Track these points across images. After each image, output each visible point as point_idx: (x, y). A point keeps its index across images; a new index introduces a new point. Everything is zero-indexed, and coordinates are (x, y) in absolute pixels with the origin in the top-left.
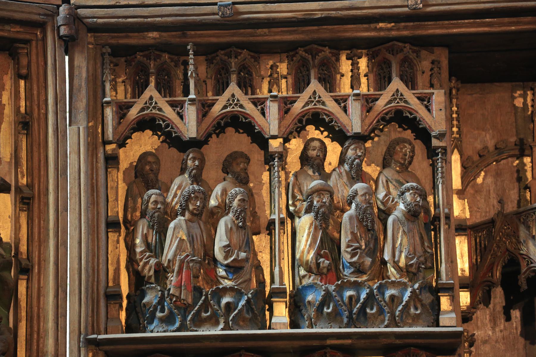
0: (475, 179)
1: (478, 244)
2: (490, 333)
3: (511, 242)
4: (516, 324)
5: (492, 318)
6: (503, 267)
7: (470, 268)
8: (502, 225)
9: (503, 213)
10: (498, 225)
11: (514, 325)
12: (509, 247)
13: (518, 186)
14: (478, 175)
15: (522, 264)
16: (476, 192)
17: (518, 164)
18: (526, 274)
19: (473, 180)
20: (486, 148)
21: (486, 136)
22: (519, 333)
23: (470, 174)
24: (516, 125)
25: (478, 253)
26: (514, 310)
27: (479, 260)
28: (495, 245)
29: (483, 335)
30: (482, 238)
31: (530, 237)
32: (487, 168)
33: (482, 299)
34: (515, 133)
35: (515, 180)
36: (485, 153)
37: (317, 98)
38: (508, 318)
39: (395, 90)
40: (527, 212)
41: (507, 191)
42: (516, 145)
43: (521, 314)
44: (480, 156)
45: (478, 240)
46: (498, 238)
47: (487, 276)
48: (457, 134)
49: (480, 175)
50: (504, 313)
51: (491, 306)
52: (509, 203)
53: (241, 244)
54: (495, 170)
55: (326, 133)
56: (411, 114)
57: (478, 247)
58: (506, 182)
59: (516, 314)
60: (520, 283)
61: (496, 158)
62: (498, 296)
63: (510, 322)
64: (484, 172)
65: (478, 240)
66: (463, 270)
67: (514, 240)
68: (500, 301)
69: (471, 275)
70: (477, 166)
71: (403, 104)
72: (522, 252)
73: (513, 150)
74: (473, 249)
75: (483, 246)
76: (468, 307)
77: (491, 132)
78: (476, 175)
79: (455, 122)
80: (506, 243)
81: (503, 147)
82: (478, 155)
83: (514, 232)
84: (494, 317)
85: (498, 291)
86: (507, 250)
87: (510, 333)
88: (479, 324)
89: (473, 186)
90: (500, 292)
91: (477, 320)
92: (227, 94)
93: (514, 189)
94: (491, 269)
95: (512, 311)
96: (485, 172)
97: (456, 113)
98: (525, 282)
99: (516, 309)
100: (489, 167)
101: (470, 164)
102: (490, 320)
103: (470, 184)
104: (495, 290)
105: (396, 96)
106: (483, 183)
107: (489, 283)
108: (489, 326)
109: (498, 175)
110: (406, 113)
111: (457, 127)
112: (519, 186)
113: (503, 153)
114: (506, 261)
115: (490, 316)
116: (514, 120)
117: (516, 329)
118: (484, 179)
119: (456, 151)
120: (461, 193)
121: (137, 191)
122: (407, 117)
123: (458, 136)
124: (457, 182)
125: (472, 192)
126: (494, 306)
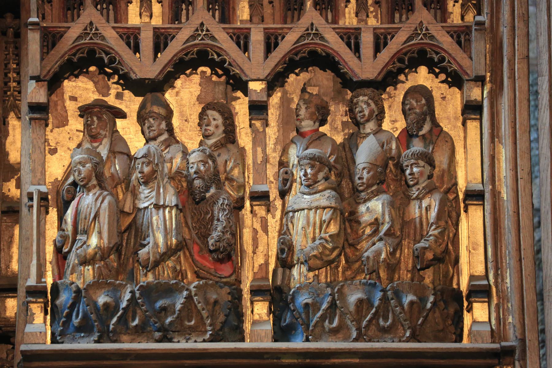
37: (93, 30)
39: (89, 22)
53: (93, 224)
55: (443, 77)
56: (219, 55)
71: (210, 42)
92: (195, 22)
105: (310, 31)
110: (100, 53)
122: (213, 59)
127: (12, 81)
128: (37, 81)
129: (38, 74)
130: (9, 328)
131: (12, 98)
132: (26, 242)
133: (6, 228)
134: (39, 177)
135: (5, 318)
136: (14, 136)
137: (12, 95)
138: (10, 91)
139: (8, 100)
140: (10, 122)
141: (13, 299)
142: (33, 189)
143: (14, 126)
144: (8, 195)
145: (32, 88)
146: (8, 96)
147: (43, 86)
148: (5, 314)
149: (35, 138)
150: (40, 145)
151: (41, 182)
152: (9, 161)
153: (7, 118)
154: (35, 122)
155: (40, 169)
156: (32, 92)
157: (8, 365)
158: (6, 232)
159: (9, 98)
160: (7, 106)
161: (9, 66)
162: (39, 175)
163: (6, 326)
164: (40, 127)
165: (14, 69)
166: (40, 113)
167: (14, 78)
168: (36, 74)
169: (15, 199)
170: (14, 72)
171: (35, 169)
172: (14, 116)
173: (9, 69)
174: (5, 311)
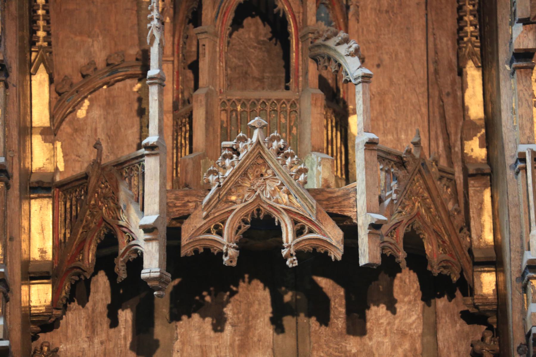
0: (74, 110)
1: (68, 210)
2: (85, 346)
3: (109, 208)
4: (125, 332)
5: (89, 323)
6: (99, 247)
7: (55, 247)
8: (98, 181)
9: (99, 164)
10: (93, 181)
11: (123, 333)
12: (106, 216)
13: (138, 123)
14: (79, 104)
15: (120, 242)
16: (76, 130)
17: (140, 90)
18: (125, 256)
19: (71, 112)
20: (92, 63)
21: (93, 45)
22: (128, 345)
23: (66, 103)
24: (139, 29)
25: (69, 225)
26: (123, 310)
27: (68, 235)
28: (88, 212)
29: (74, 350)
30: (74, 202)
31: (133, 201)
32: (93, 95)
33: (73, 289)
34: (137, 42)
35: (134, 113)
36: (89, 72)
38: (114, 323)
40: (131, 163)
41: (122, 130)
42: (137, 59)
43: (133, 316)
44: (84, 76)
45: (68, 205)
46: (93, 202)
47: (77, 259)
48: (44, 41)
49: (82, 106)
50: (109, 316)
51: (89, 305)
52: (125, 148)
54: (105, 98)
57: (68, 215)
58: (122, 115)
59: (126, 316)
60: (116, 270)
61: (107, 79)
62: (101, 289)
63: (116, 329)
64: (89, 100)
65: (68, 205)
66: (43, 251)
67: (112, 205)
68: (104, 297)
69: (56, 258)
70: (77, 92)
72: (121, 223)
73: (132, 66)
74: (61, 219)
75: (74, 213)
76: (47, 308)
77: (100, 38)
78: (76, 105)
79: (41, 23)
80: (102, 210)
81: (117, 63)
82: (80, 75)
83: (113, 193)
84: (92, 322)
85: (102, 283)
86: (104, 220)
87: (116, 345)
88: (70, 332)
89: (71, 123)
90: (105, 283)
91: (67, 327)
93: (133, 126)
94: (81, 248)
95: (120, 311)
96: (91, 101)
97: (43, 9)
98: (124, 268)
99: (127, 308)
100: (97, 92)
101: (67, 88)
102: (87, 327)
103: (67, 120)
104: (97, 280)
106: (86, 117)
107: (78, 270)
108: (84, 335)
109: (110, 104)
111: (44, 31)
112: (141, 123)
113: (117, 71)
114: (103, 237)
115: (87, 320)
116: (136, 22)
117: (125, 338)
118: (88, 112)
119: (42, 66)
120: (50, 134)
121: (296, 132)
123: (45, 44)
124: (40, 115)
125: (69, 130)
126: (95, 304)
127: (469, 25)
128: (524, 24)
129: (529, 16)
130: (487, 307)
131: (470, 45)
132: (514, 210)
133: (474, 193)
134: (528, 135)
135: (482, 296)
136: (473, 88)
137: (470, 41)
138: (466, 36)
139: (466, 48)
140: (469, 72)
141: (489, 274)
142: (523, 148)
143: (473, 76)
144: (471, 156)
145: (519, 33)
146: (465, 43)
147: (531, 29)
148: (482, 290)
149: (521, 90)
150: (528, 98)
151: (531, 141)
152: (469, 117)
153: (465, 67)
154: (521, 72)
155: (529, 125)
156: (519, 36)
157: (487, 349)
158: (474, 198)
159: (467, 45)
160: (464, 55)
161: (465, 8)
162: (527, 132)
163: (484, 305)
164: (526, 77)
165: (471, 11)
166: (526, 61)
167: (471, 21)
168: (525, 16)
169: (480, 160)
170: (471, 14)
171: (523, 125)
172: (473, 65)
173: (465, 12)
174: (482, 287)
